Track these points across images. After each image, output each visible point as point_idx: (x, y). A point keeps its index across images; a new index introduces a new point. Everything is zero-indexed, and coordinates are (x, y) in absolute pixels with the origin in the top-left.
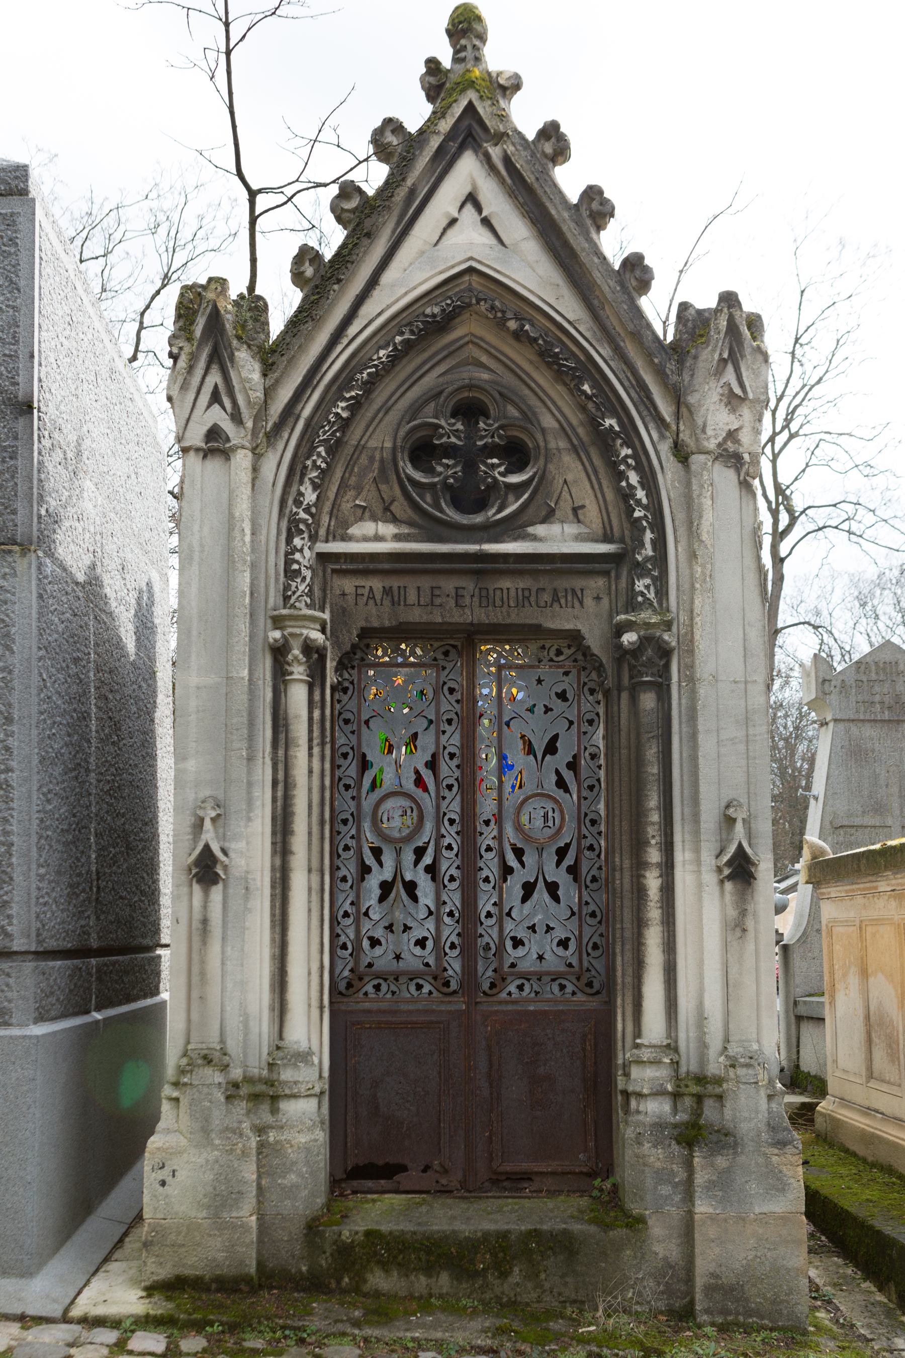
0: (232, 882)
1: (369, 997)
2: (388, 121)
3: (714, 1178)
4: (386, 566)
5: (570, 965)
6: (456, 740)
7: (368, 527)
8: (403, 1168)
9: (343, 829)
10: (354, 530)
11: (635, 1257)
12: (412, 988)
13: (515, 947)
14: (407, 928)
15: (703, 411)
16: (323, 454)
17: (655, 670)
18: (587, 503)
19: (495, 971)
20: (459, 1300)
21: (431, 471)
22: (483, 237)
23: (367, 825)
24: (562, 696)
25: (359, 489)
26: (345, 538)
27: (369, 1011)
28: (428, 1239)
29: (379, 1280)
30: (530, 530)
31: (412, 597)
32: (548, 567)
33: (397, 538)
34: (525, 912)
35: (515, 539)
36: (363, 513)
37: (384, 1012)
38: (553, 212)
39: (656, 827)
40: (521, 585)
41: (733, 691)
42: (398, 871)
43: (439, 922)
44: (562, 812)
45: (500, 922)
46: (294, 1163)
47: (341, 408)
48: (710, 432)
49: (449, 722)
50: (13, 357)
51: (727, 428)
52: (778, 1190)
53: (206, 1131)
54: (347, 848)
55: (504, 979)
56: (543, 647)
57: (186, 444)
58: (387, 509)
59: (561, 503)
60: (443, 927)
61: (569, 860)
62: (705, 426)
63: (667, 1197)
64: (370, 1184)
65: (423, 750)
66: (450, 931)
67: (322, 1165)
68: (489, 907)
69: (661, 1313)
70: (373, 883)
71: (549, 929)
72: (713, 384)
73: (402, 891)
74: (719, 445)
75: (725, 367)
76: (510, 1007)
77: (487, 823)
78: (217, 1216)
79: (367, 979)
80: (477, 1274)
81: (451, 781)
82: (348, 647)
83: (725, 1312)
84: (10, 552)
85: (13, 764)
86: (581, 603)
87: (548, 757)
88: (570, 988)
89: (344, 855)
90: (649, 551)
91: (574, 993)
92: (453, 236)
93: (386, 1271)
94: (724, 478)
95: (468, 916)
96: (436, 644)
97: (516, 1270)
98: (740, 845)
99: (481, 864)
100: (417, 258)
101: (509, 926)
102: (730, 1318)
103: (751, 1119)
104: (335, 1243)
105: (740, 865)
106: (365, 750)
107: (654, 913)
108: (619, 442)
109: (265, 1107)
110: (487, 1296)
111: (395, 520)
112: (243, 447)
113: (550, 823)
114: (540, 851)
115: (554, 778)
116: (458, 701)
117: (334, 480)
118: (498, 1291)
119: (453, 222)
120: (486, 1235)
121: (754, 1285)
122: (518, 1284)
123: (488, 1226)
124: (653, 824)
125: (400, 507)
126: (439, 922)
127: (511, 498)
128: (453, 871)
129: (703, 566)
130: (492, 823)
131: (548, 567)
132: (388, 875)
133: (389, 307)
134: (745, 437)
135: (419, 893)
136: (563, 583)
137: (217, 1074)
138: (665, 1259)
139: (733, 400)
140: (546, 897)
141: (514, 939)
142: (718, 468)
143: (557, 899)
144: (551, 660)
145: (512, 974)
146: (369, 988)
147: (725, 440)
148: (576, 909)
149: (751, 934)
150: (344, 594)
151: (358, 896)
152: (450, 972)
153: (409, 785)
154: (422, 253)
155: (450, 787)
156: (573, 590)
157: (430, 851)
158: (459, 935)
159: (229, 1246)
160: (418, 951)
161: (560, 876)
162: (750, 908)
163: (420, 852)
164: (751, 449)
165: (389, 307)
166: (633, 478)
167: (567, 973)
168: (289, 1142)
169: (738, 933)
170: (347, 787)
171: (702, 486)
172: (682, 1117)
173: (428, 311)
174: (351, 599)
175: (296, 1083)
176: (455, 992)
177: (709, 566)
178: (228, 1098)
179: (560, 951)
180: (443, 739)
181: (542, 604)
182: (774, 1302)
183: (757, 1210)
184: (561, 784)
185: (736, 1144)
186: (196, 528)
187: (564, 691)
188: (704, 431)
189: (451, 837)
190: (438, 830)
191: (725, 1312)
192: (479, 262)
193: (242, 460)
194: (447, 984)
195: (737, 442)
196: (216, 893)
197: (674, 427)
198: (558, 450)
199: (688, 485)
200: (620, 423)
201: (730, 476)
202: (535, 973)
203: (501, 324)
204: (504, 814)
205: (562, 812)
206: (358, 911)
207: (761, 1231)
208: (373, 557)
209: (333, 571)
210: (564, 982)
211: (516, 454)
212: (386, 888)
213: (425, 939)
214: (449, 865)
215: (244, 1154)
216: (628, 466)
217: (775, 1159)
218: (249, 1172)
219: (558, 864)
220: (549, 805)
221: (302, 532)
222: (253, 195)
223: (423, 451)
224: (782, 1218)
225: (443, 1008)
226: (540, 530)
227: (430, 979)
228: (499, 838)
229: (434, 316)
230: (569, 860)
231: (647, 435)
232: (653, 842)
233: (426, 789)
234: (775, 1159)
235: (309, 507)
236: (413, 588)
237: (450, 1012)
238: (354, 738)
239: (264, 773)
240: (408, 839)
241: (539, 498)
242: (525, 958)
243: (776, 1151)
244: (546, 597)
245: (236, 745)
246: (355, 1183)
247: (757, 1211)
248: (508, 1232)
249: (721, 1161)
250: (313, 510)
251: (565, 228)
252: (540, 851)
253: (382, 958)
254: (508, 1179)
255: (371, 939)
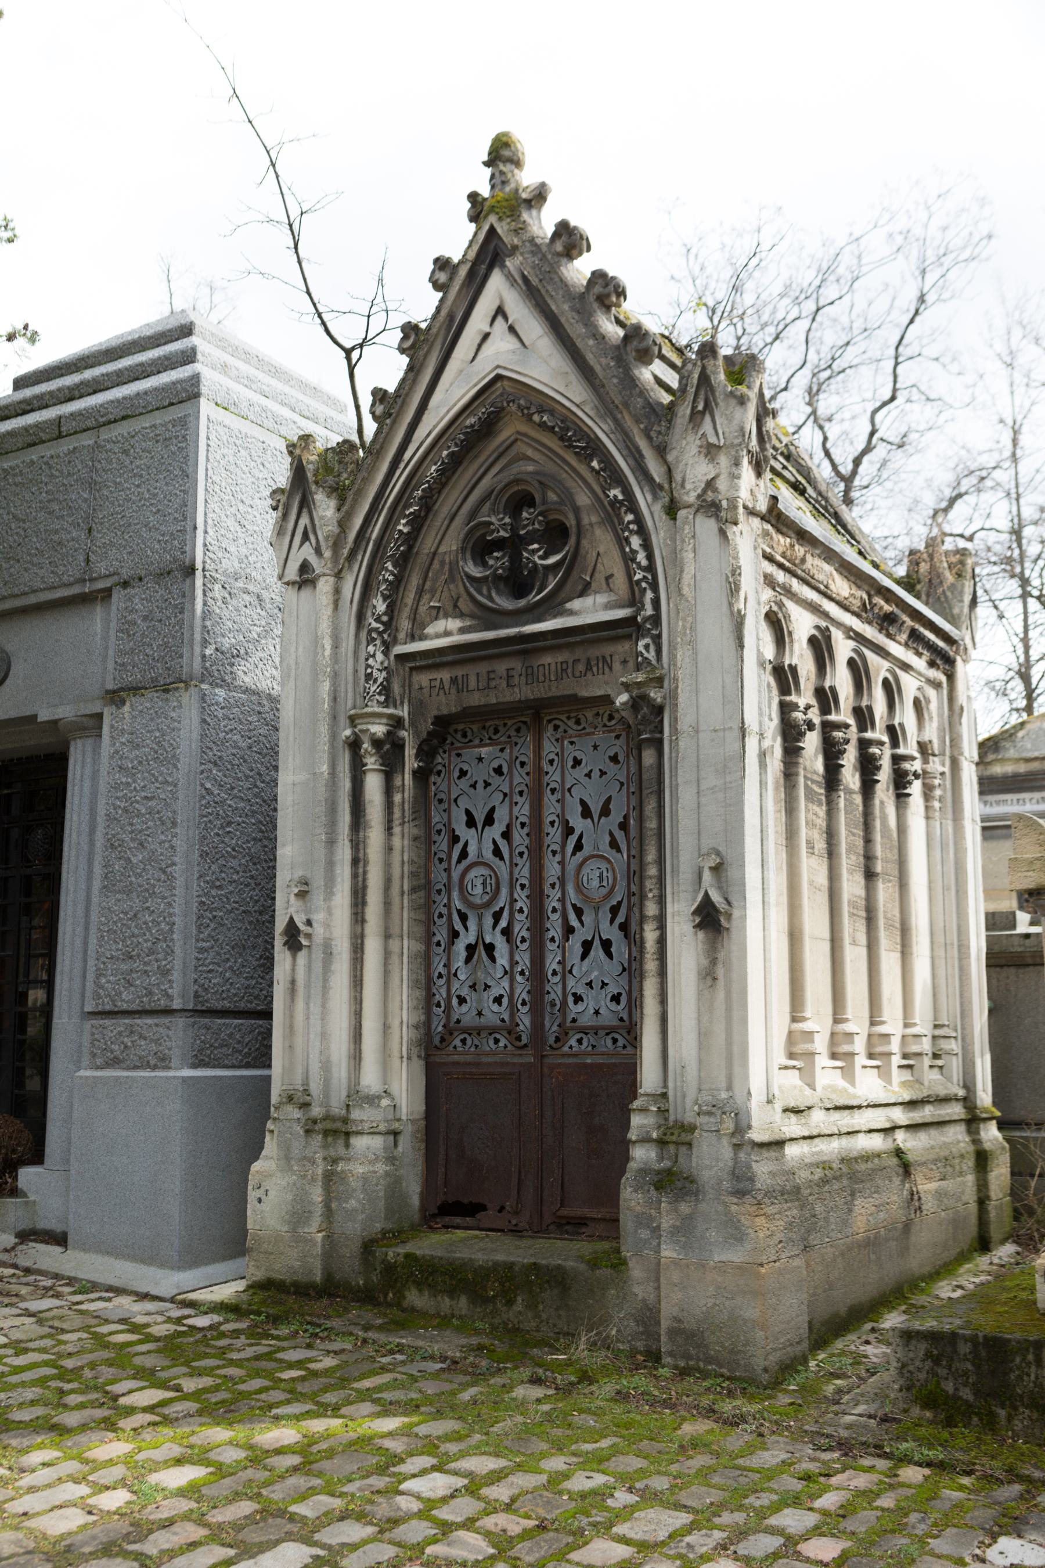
0: (314, 947)
1: (459, 1050)
2: (437, 261)
3: (678, 1223)
4: (450, 658)
5: (621, 1020)
6: (526, 810)
7: (440, 625)
8: (483, 1208)
9: (437, 898)
10: (430, 630)
11: (618, 1297)
12: (491, 1042)
13: (576, 1003)
14: (487, 987)
15: (681, 466)
16: (390, 568)
17: (652, 727)
18: (615, 571)
19: (559, 1026)
20: (474, 1322)
21: (485, 564)
22: (511, 343)
23: (455, 894)
24: (614, 759)
25: (433, 592)
26: (423, 638)
27: (458, 1063)
28: (451, 1264)
29: (415, 1298)
30: (568, 605)
31: (473, 684)
32: (578, 639)
33: (462, 631)
34: (584, 969)
35: (555, 617)
36: (438, 613)
37: (470, 1064)
38: (554, 308)
39: (654, 881)
40: (560, 659)
41: (713, 740)
42: (480, 935)
43: (512, 980)
44: (614, 871)
45: (564, 980)
46: (354, 1190)
47: (403, 526)
48: (688, 486)
49: (521, 793)
50: (183, 531)
51: (705, 479)
52: (736, 1239)
53: (287, 1158)
54: (441, 916)
55: (567, 1034)
56: (598, 714)
57: (285, 580)
58: (455, 606)
59: (597, 575)
60: (516, 985)
61: (620, 919)
62: (684, 481)
63: (646, 1241)
64: (458, 1220)
65: (500, 822)
66: (522, 990)
67: (381, 1194)
68: (555, 966)
69: (640, 1353)
70: (460, 946)
71: (604, 985)
72: (691, 438)
73: (483, 953)
74: (699, 496)
75: (703, 419)
76: (571, 1060)
77: (553, 886)
78: (294, 1230)
79: (456, 1033)
80: (487, 1300)
81: (522, 849)
82: (424, 735)
83: (687, 1357)
84: (177, 689)
85: (176, 859)
86: (611, 668)
87: (603, 819)
88: (621, 1042)
89: (439, 922)
90: (649, 611)
91: (624, 1047)
92: (488, 350)
93: (420, 1291)
94: (706, 526)
95: (537, 974)
96: (510, 723)
97: (519, 1299)
98: (706, 894)
99: (548, 925)
100: (456, 378)
101: (571, 983)
102: (691, 1363)
103: (711, 1168)
104: (383, 1261)
105: (708, 915)
106: (454, 826)
107: (651, 965)
108: (623, 509)
109: (341, 1141)
110: (496, 1321)
111: (462, 615)
112: (324, 575)
113: (605, 883)
114: (596, 909)
115: (607, 839)
116: (528, 774)
117: (409, 587)
118: (505, 1316)
119: (486, 336)
120: (496, 1264)
121: (713, 1333)
122: (520, 1312)
123: (500, 1257)
124: (651, 877)
125: (464, 605)
126: (512, 980)
127: (551, 578)
128: (524, 933)
129: (684, 620)
130: (557, 886)
131: (578, 639)
132: (471, 939)
133: (435, 427)
134: (722, 485)
135: (496, 954)
136: (595, 652)
137: (296, 1110)
138: (644, 1300)
139: (711, 451)
140: (601, 953)
141: (574, 995)
142: (700, 519)
143: (610, 955)
144: (605, 726)
145: (572, 1029)
146: (457, 1042)
147: (704, 491)
148: (626, 965)
149: (721, 982)
150: (421, 688)
151: (449, 959)
152: (522, 1027)
153: (488, 854)
154: (461, 371)
155: (521, 854)
156: (604, 658)
157: (506, 914)
158: (529, 992)
159: (300, 1258)
160: (495, 1007)
161: (611, 932)
162: (721, 955)
163: (497, 916)
164: (728, 495)
165: (435, 427)
166: (636, 542)
167: (618, 1027)
168: (351, 1171)
169: (709, 982)
170: (441, 860)
171: (683, 541)
172: (666, 1164)
173: (468, 423)
174: (426, 691)
175: (362, 1121)
176: (526, 1046)
177: (690, 619)
178: (307, 1132)
179: (613, 1006)
180: (516, 809)
181: (578, 674)
182: (731, 1352)
183: (717, 1258)
184: (614, 844)
185: (697, 1193)
186: (293, 649)
187: (616, 754)
188: (683, 486)
189: (522, 902)
190: (512, 895)
191: (687, 1357)
192: (505, 368)
193: (325, 585)
194: (519, 1038)
195: (715, 490)
196: (302, 957)
197: (666, 486)
198: (591, 525)
199: (674, 540)
200: (623, 493)
201: (711, 524)
202: (592, 1028)
203: (529, 417)
204: (567, 877)
205: (614, 871)
206: (449, 972)
207: (720, 1279)
208: (440, 651)
209: (411, 669)
210: (616, 1036)
211: (556, 534)
212: (471, 949)
213: (502, 996)
214: (521, 930)
215: (313, 1180)
216: (631, 531)
217: (734, 1208)
218: (317, 1195)
219: (612, 922)
220: (604, 866)
221: (374, 639)
222: (348, 352)
223: (481, 547)
224: (739, 1268)
225: (515, 1060)
226: (576, 604)
227: (505, 1033)
228: (562, 900)
229: (472, 426)
230: (620, 919)
231: (642, 498)
232: (650, 895)
233: (502, 858)
234: (734, 1208)
235: (379, 616)
236: (473, 674)
237: (521, 1064)
238: (445, 816)
239: (344, 853)
240: (488, 905)
241: (575, 574)
242: (583, 1012)
243: (735, 1200)
244: (581, 667)
245: (318, 831)
246: (447, 1219)
247: (716, 1259)
248: (513, 1263)
249: (684, 1208)
250: (385, 618)
251: (563, 320)
252: (596, 909)
253: (465, 1013)
254: (568, 1223)
255: (459, 997)
